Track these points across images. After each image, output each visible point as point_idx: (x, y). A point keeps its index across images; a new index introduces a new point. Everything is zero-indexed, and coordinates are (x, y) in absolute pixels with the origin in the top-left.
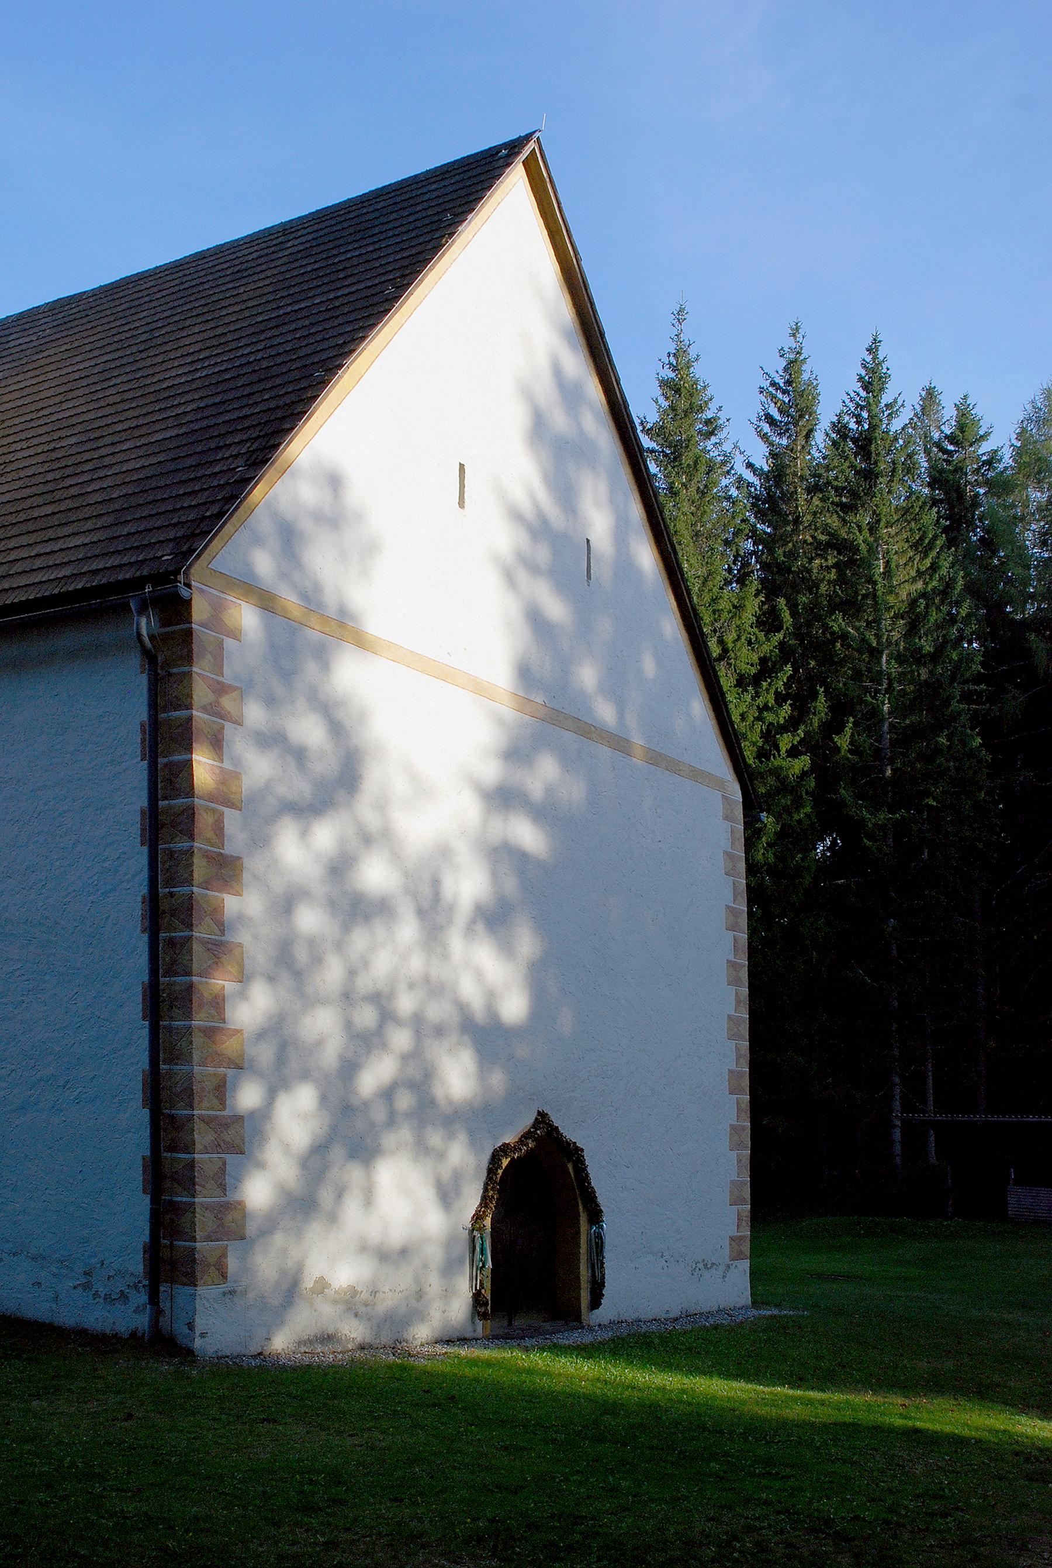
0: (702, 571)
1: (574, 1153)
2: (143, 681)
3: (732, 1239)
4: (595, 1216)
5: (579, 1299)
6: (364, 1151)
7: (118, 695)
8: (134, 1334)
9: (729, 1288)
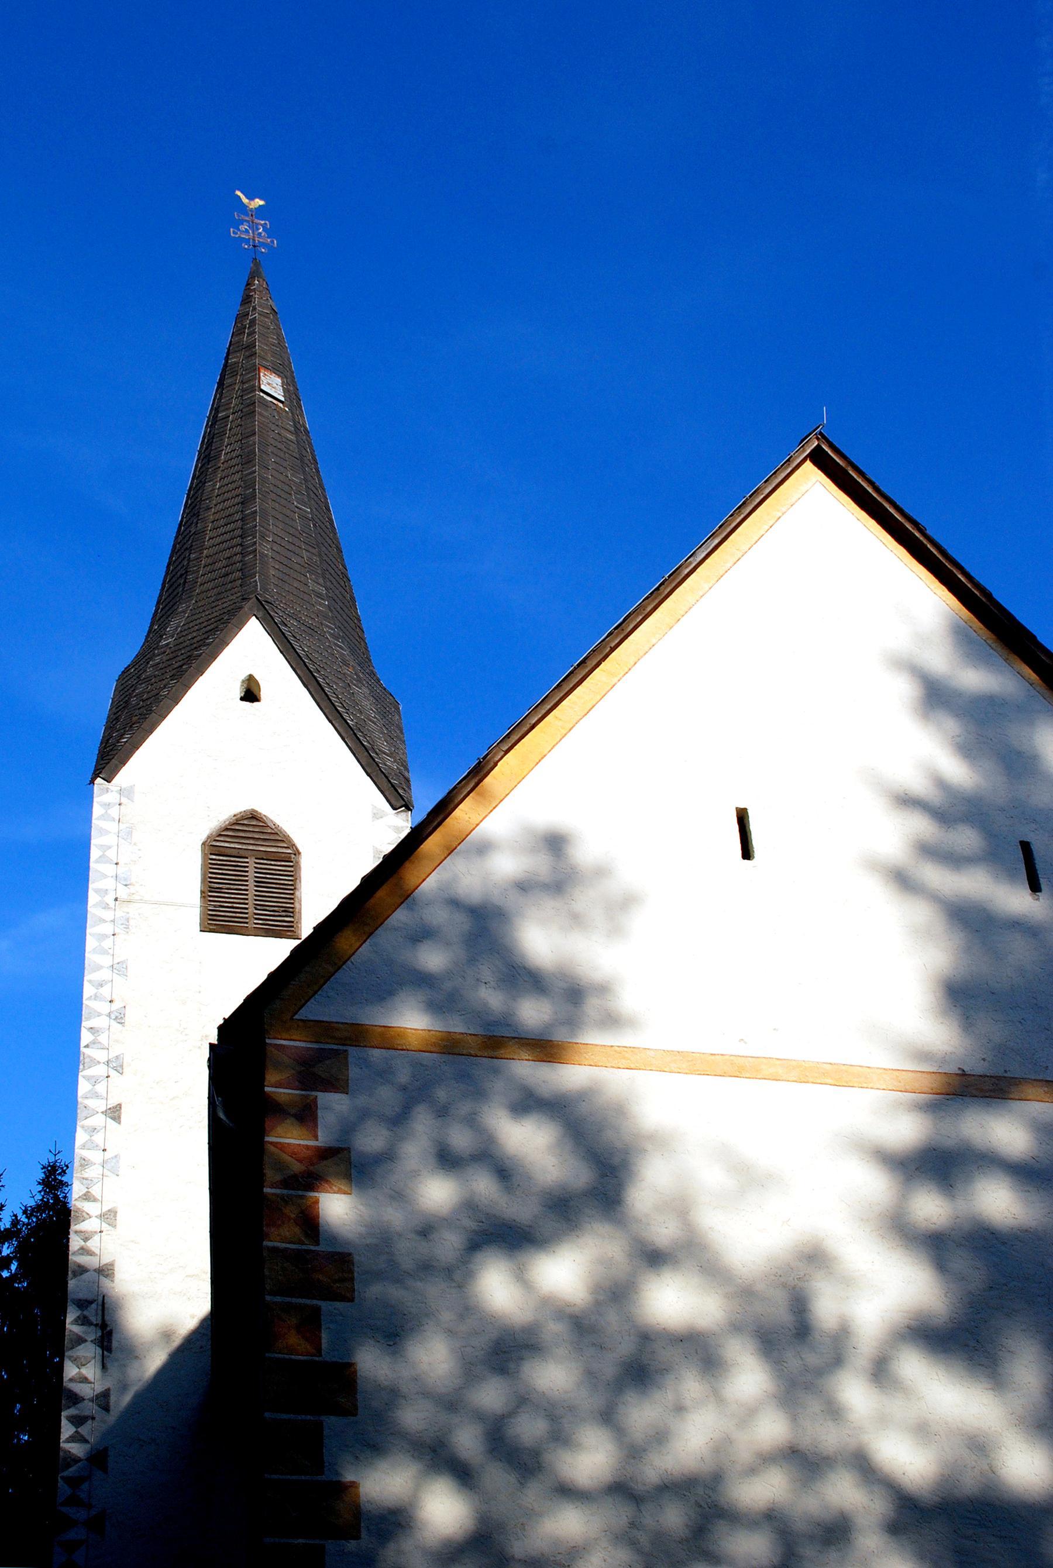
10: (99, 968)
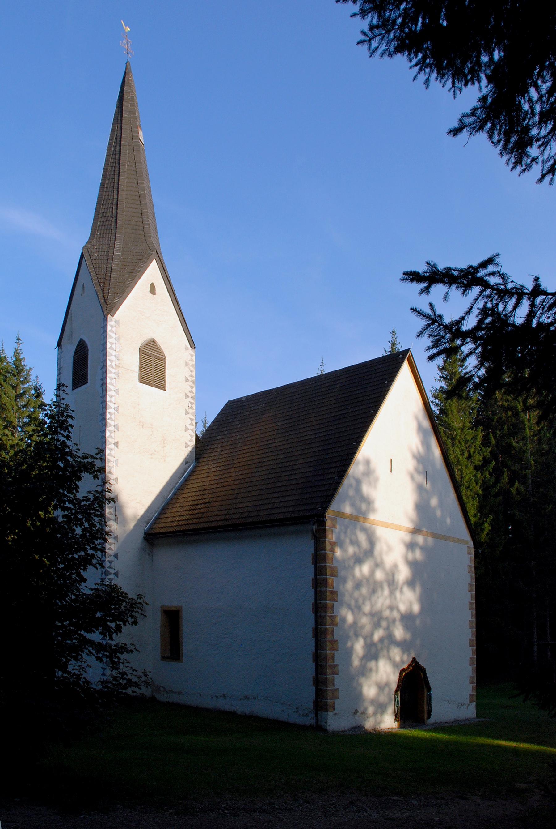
0: (461, 425)
1: (423, 670)
2: (312, 543)
3: (470, 695)
4: (429, 689)
5: (424, 716)
6: (375, 657)
7: (304, 547)
8: (310, 725)
9: (469, 712)
10: (111, 390)
